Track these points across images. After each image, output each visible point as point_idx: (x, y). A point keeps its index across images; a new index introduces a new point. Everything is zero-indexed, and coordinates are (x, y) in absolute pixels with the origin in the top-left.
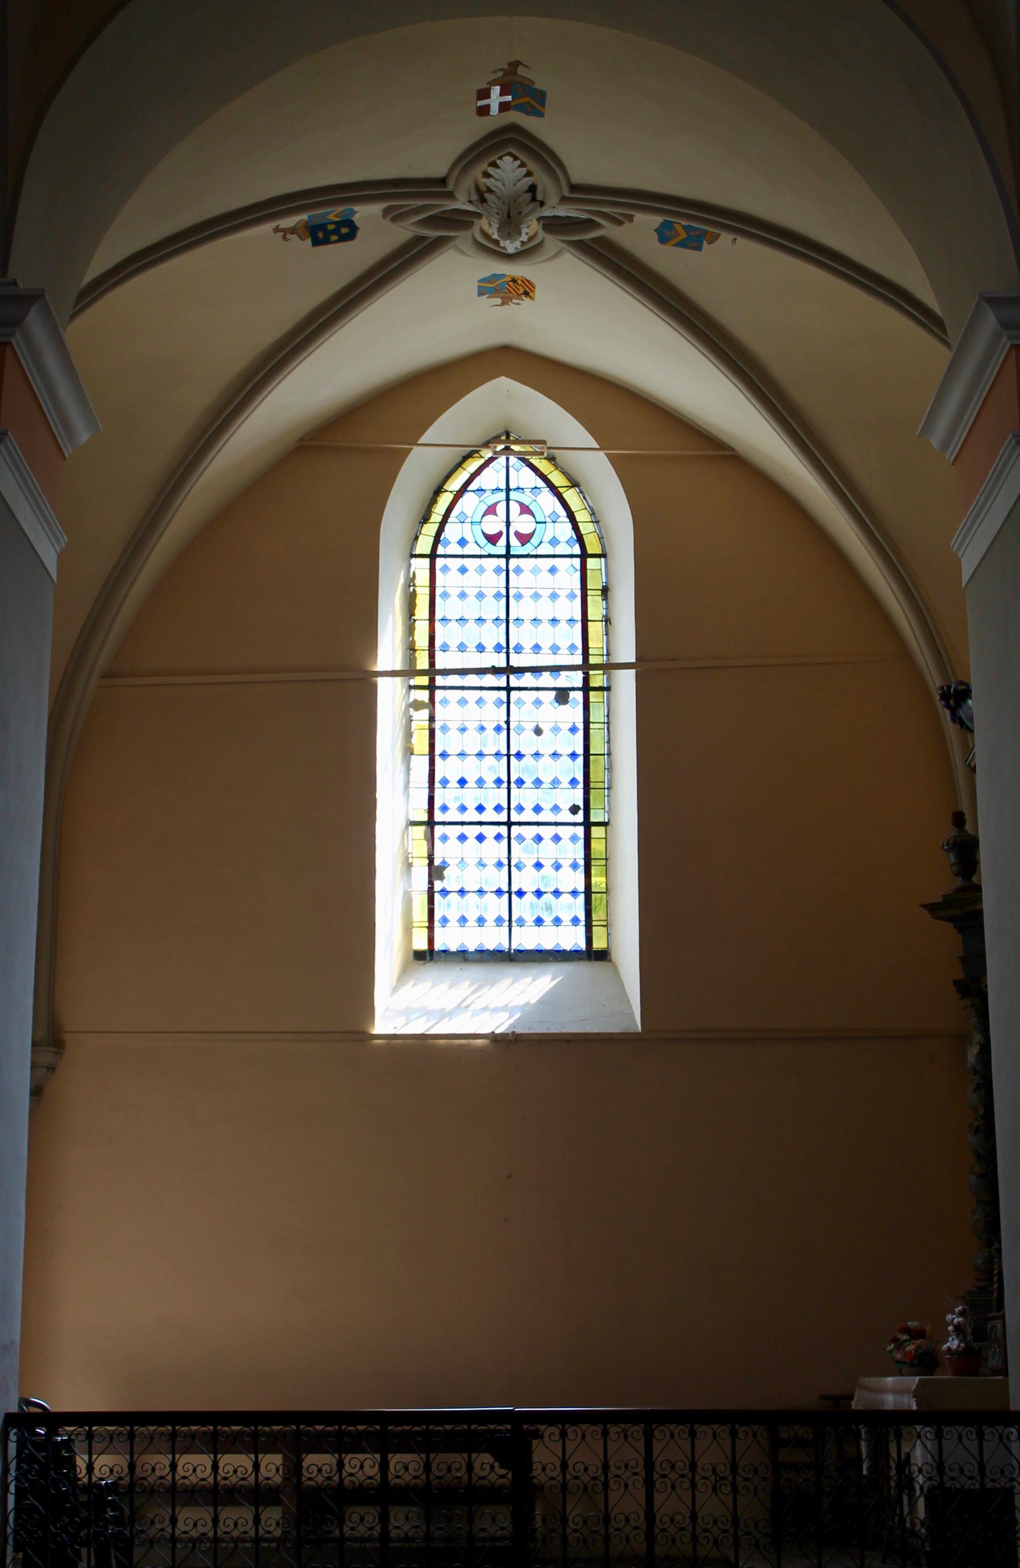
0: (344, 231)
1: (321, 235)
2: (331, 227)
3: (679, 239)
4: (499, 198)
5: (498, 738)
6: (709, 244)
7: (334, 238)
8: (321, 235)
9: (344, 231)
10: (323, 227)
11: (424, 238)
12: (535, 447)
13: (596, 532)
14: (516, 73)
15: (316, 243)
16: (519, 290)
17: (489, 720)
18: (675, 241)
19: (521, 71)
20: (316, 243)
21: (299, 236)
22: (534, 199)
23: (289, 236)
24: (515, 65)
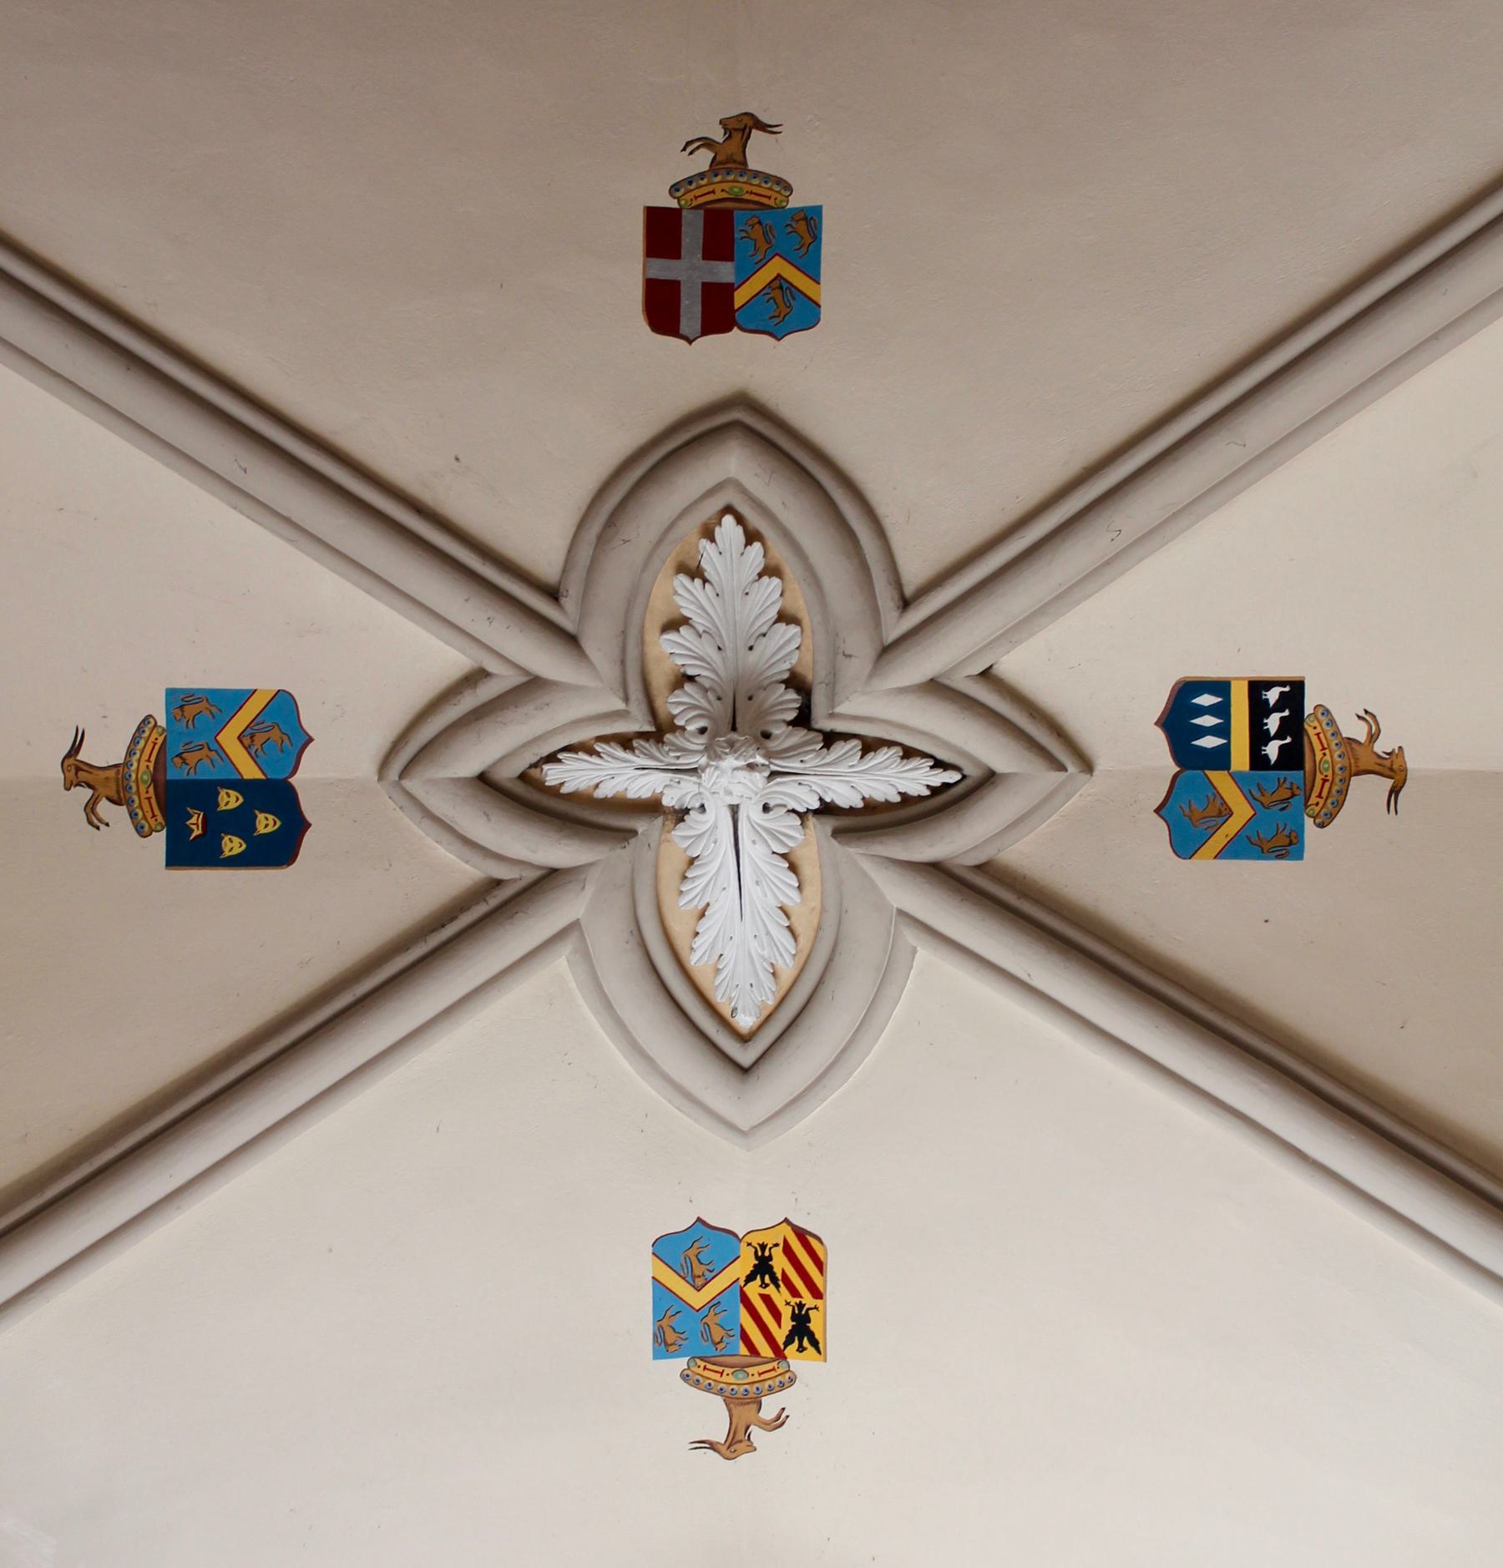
0: (266, 824)
1: (195, 824)
2: (229, 800)
3: (1232, 827)
4: (706, 690)
5: (774, 599)
6: (1322, 826)
7: (233, 845)
8: (195, 824)
9: (266, 824)
10: (203, 793)
11: (497, 883)
12: (878, 771)
13: (1291, 789)
14: (745, 163)
15: (183, 854)
16: (777, 1315)
17: (662, 1287)
18: (1219, 840)
19: (760, 154)
20: (183, 854)
21: (133, 815)
22: (803, 719)
23: (105, 808)
24: (743, 127)
